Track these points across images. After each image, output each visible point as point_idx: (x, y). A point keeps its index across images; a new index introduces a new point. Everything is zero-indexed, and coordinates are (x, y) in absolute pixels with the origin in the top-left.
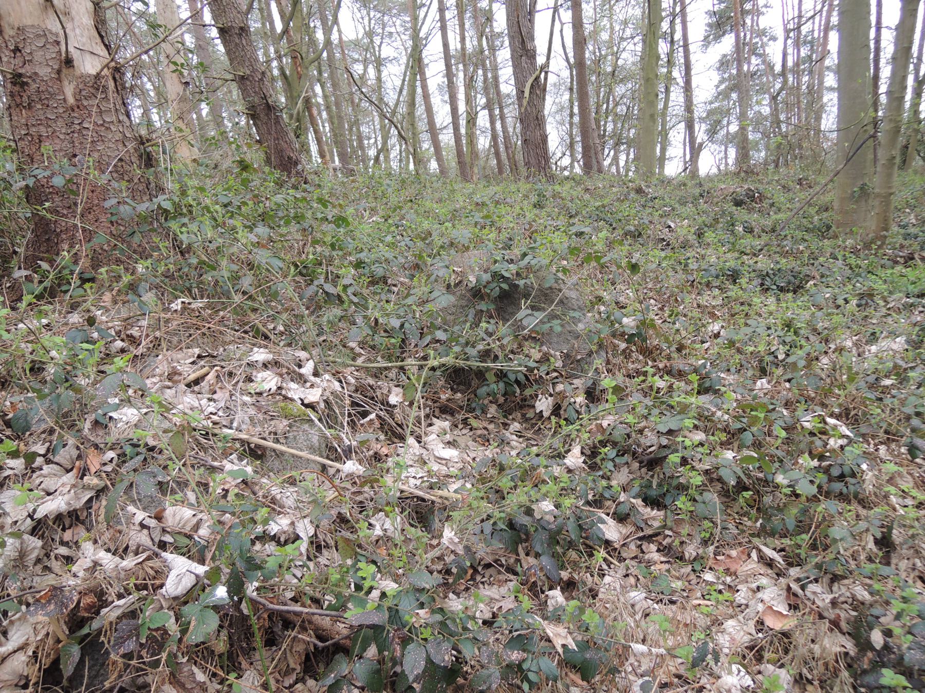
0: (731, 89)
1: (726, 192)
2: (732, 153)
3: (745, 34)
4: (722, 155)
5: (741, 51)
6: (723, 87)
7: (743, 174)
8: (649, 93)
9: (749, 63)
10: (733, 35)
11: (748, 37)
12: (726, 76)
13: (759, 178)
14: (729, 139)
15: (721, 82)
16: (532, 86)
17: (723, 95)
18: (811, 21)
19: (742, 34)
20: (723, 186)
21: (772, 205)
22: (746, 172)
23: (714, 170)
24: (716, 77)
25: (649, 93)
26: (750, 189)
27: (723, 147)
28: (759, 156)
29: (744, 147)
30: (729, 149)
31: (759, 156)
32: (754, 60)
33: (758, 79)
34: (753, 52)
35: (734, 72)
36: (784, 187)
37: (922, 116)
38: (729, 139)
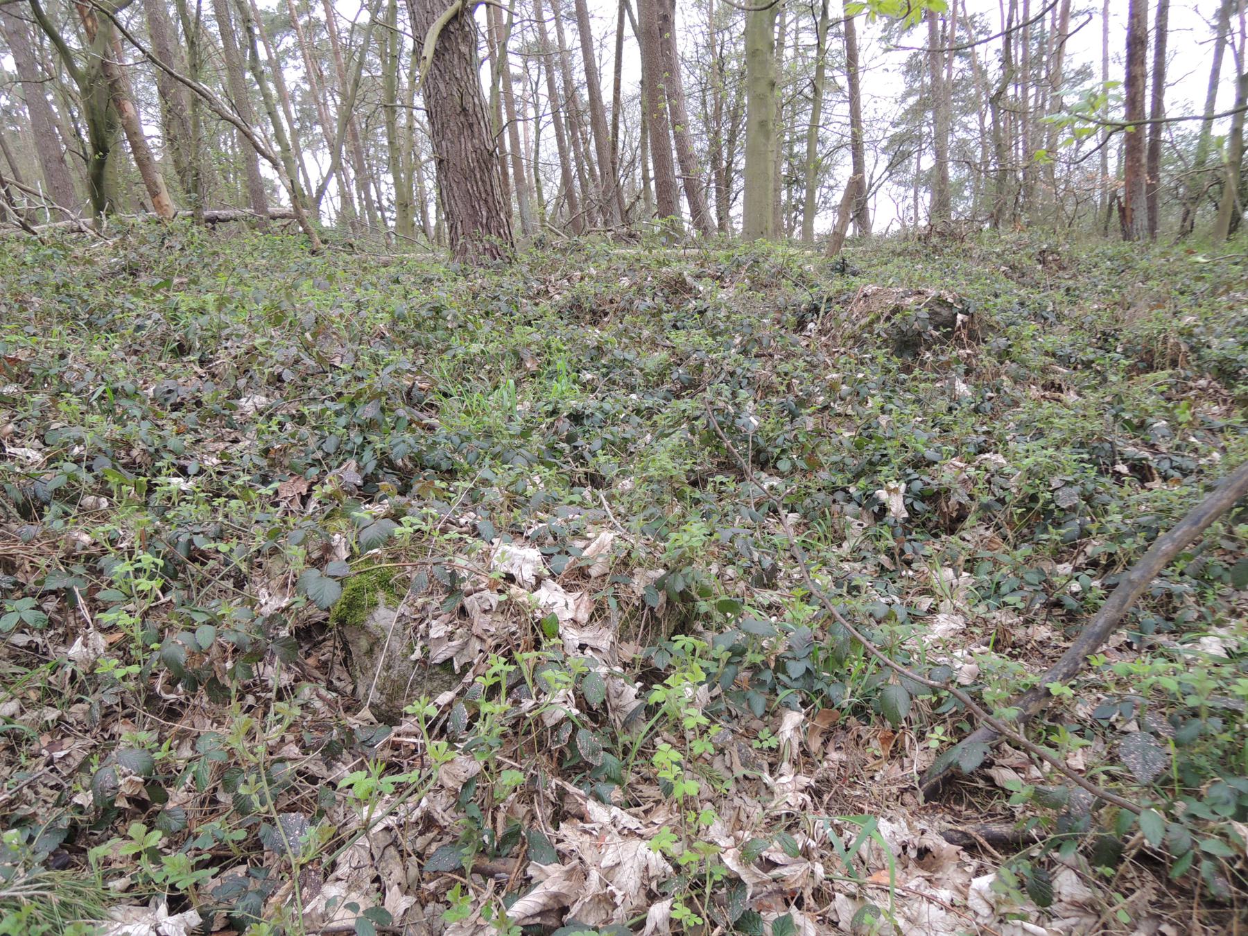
0: (922, 106)
1: (876, 307)
2: (926, 198)
3: (944, 27)
4: (910, 201)
5: (938, 50)
6: (912, 100)
7: (935, 240)
8: (757, 79)
9: (950, 68)
10: (926, 24)
11: (949, 28)
12: (917, 85)
13: (966, 246)
14: (919, 180)
15: (908, 94)
16: (445, 33)
17: (915, 113)
18: (1032, 17)
19: (940, 23)
20: (870, 289)
21: (1004, 355)
22: (941, 234)
23: (896, 227)
24: (899, 84)
25: (757, 79)
26: (940, 301)
27: (911, 192)
28: (963, 206)
29: (938, 182)
30: (921, 194)
31: (963, 206)
32: (958, 63)
33: (962, 91)
34: (958, 50)
35: (927, 80)
36: (1013, 268)
37: (1245, 137)
38: (919, 180)
